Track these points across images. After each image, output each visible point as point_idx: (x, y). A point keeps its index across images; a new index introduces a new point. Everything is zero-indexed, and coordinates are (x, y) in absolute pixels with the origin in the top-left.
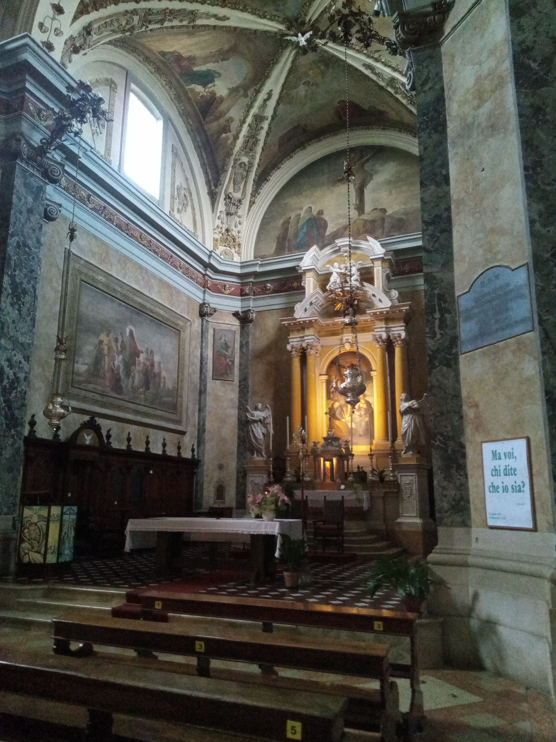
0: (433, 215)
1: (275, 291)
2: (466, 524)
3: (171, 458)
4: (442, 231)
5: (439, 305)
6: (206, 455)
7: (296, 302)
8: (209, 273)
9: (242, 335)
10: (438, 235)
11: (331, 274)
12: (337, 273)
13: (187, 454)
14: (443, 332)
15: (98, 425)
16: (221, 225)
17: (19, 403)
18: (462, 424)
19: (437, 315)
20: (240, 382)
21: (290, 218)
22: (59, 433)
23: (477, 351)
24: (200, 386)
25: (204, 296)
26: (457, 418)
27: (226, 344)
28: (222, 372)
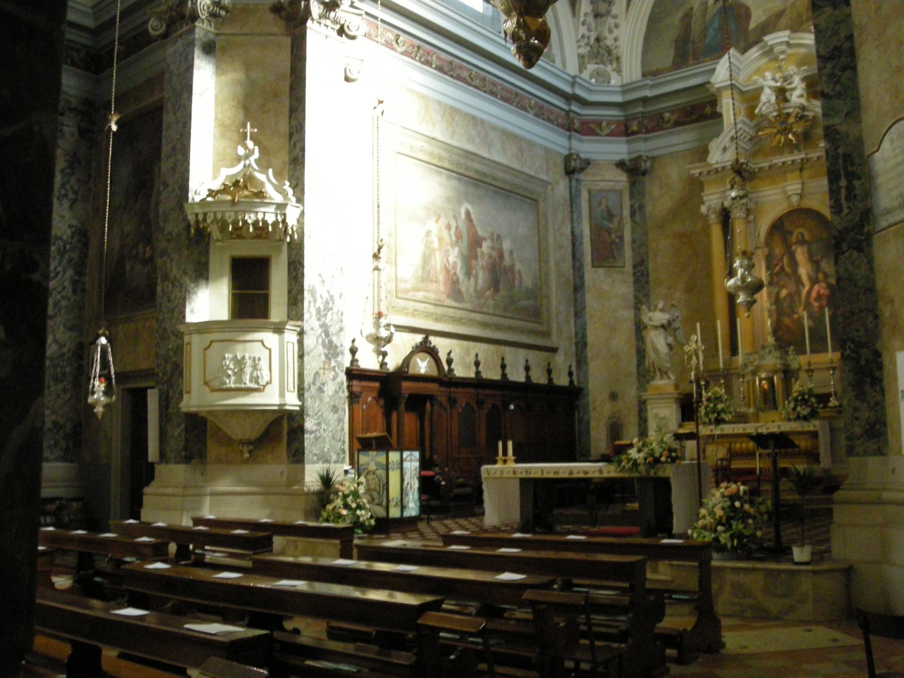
0: (832, 47)
1: (677, 124)
2: (880, 452)
3: (538, 387)
4: (844, 69)
5: (845, 168)
6: (590, 381)
7: (711, 138)
8: (575, 107)
9: (632, 196)
10: (839, 73)
11: (761, 89)
12: (770, 87)
13: (562, 380)
14: (851, 206)
15: (434, 347)
16: (587, 33)
17: (337, 327)
18: (877, 326)
19: (843, 183)
20: (634, 267)
21: (692, 8)
22: (387, 360)
23: (890, 229)
24: (574, 280)
25: (570, 143)
26: (870, 318)
27: (609, 211)
28: (606, 253)
